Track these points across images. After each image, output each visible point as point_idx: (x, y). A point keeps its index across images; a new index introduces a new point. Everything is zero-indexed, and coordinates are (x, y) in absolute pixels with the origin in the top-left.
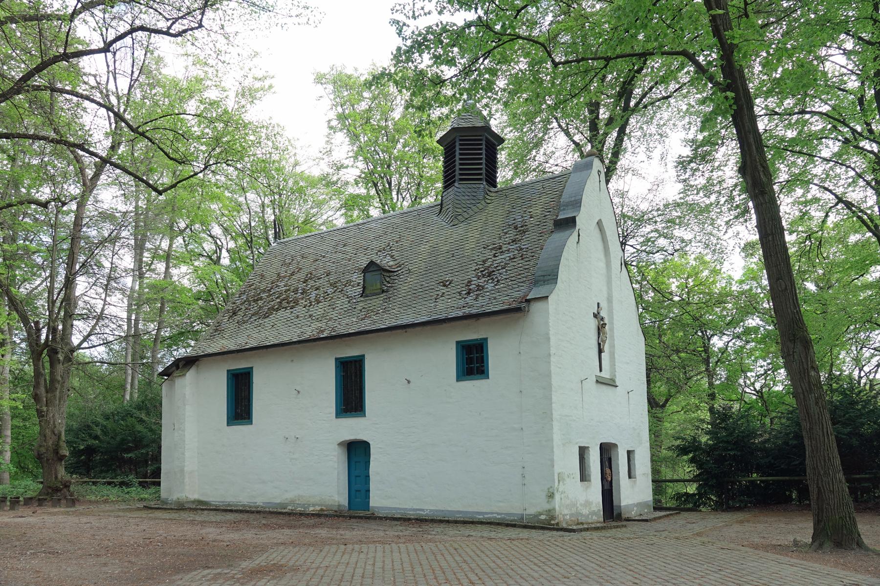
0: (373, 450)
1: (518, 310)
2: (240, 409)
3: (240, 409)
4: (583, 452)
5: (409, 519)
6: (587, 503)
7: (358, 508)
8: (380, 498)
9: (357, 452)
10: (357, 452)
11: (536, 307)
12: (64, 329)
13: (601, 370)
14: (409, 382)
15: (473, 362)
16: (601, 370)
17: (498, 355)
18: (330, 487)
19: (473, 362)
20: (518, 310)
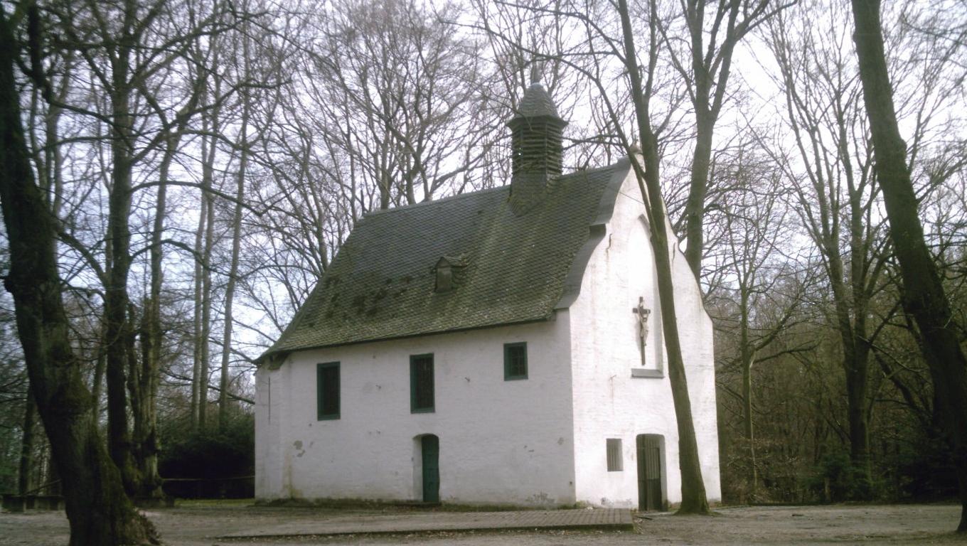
0: (441, 444)
1: (544, 320)
2: (329, 405)
3: (329, 405)
4: (613, 448)
5: (310, 535)
6: (629, 502)
7: (430, 499)
8: (447, 491)
9: (429, 445)
10: (429, 445)
11: (561, 315)
12: (200, 283)
13: (643, 362)
14: (469, 380)
15: (516, 364)
16: (643, 362)
17: (535, 358)
18: (402, 477)
19: (516, 364)
20: (544, 320)
